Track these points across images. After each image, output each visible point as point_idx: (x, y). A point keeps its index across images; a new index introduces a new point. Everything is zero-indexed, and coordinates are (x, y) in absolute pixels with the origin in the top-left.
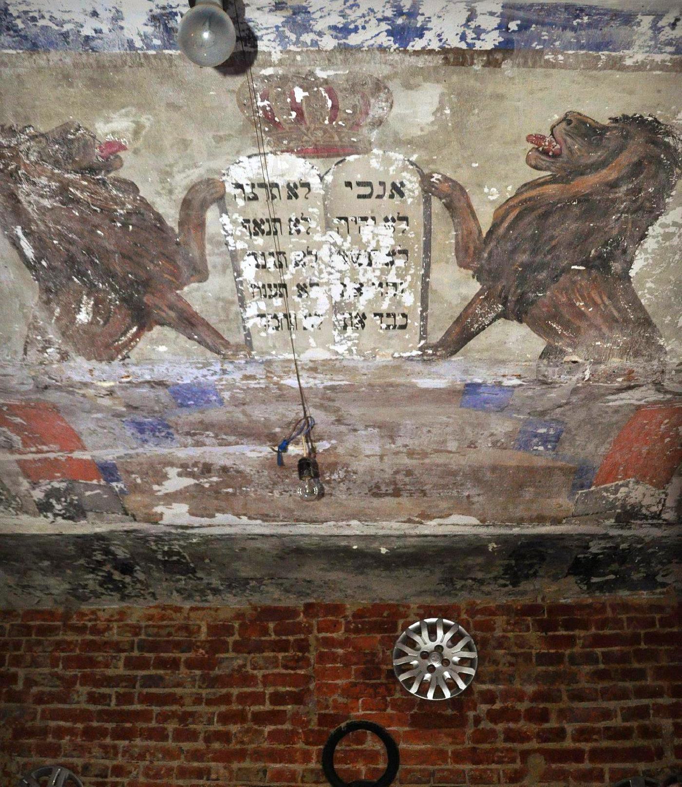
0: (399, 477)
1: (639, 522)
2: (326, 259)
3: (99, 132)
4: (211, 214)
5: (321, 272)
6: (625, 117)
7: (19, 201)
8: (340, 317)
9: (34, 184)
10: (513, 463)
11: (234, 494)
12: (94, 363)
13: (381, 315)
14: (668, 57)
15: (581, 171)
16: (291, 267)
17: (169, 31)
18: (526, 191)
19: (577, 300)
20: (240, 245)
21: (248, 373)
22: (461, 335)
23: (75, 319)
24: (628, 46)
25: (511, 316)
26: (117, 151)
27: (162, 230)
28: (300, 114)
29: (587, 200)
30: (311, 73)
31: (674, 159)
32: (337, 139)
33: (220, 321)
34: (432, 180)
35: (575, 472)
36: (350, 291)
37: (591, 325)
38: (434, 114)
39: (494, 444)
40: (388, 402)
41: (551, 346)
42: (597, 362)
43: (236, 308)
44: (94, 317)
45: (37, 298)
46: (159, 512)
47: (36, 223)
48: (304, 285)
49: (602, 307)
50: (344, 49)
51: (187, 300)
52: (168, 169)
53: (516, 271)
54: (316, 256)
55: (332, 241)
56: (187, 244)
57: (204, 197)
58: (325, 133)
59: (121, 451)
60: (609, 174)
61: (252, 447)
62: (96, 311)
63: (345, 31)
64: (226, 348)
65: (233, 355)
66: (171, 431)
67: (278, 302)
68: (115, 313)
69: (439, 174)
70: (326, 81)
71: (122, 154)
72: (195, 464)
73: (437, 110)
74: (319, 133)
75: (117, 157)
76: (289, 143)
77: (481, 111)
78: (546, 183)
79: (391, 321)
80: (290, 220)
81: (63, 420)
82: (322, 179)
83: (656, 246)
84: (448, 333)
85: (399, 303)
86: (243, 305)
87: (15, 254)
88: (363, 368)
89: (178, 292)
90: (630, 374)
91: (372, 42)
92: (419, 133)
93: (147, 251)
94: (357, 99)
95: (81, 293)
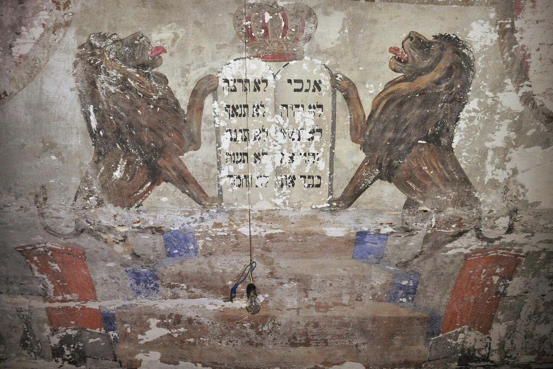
0: (310, 328)
1: (474, 364)
2: (273, 135)
3: (153, 39)
4: (208, 100)
6: (441, 35)
7: (96, 87)
8: (279, 178)
9: (108, 75)
10: (386, 314)
11: (194, 344)
12: (119, 208)
13: (305, 177)
15: (419, 73)
16: (252, 140)
18: (389, 87)
19: (424, 166)
20: (223, 124)
21: (217, 221)
22: (354, 192)
23: (112, 175)
26: (161, 53)
27: (177, 111)
28: (267, 31)
29: (424, 94)
31: (469, 64)
32: (285, 49)
34: (337, 79)
35: (428, 322)
36: (287, 159)
37: (434, 184)
39: (374, 296)
40: (306, 254)
41: (410, 199)
42: (439, 211)
43: (215, 170)
44: (125, 174)
45: (91, 159)
46: (139, 359)
47: (103, 104)
48: (259, 154)
49: (438, 170)
51: (185, 163)
53: (386, 145)
54: (267, 132)
55: (277, 122)
57: (206, 88)
59: (120, 302)
60: (435, 75)
61: (211, 300)
62: (126, 171)
64: (206, 200)
65: (210, 205)
66: (158, 282)
67: (241, 166)
69: (341, 74)
71: (163, 56)
72: (170, 317)
73: (341, 30)
74: (276, 45)
76: (258, 51)
77: (365, 30)
78: (400, 81)
79: (310, 181)
80: (254, 106)
81: (86, 268)
82: (274, 77)
83: (465, 126)
84: (346, 190)
85: (316, 168)
86: (219, 169)
87: (85, 125)
88: (292, 217)
89: (180, 157)
90: (459, 222)
92: (331, 46)
93: (166, 125)
94: (298, 22)
95: (120, 156)
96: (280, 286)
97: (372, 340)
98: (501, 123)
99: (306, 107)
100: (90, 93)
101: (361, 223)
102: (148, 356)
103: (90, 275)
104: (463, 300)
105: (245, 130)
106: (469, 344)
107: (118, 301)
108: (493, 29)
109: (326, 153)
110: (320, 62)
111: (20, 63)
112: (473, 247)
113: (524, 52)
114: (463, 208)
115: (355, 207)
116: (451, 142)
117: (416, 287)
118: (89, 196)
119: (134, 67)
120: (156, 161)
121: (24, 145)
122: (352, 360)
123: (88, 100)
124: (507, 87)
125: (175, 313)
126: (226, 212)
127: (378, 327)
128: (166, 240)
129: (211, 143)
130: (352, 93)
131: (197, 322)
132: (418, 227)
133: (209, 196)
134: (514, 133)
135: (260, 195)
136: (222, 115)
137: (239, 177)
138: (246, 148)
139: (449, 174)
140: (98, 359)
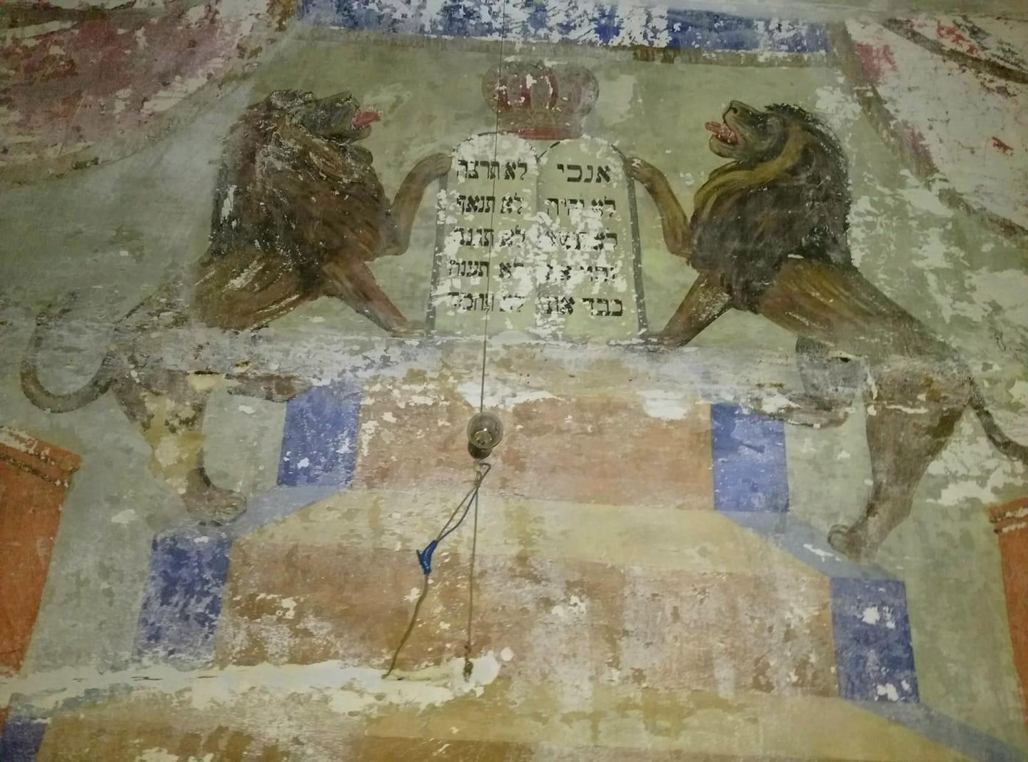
2: (534, 239)
3: (365, 103)
4: (431, 189)
6: (777, 106)
7: (254, 161)
8: (544, 300)
13: (591, 301)
17: (452, 20)
20: (450, 220)
21: (416, 366)
24: (756, 45)
25: (742, 306)
27: (377, 200)
28: (528, 99)
30: (541, 62)
32: (554, 123)
33: (402, 298)
36: (557, 274)
37: (842, 318)
38: (630, 102)
43: (426, 285)
44: (252, 283)
50: (565, 42)
52: (407, 142)
54: (524, 235)
55: (541, 222)
56: (397, 215)
62: (257, 278)
63: (567, 28)
64: (400, 324)
67: (475, 281)
70: (551, 70)
71: (373, 124)
74: (541, 117)
79: (603, 307)
80: (504, 199)
82: (538, 160)
85: (611, 289)
86: (435, 280)
88: (570, 362)
89: (367, 263)
91: (585, 37)
101: (715, 383)
103: (48, 559)
105: (487, 231)
108: (849, 98)
112: (997, 479)
115: (696, 346)
117: (907, 634)
119: (325, 138)
120: (319, 267)
123: (232, 177)
125: (233, 727)
126: (439, 347)
129: (426, 245)
132: (843, 397)
137: (470, 296)
138: (487, 255)
139: (866, 304)
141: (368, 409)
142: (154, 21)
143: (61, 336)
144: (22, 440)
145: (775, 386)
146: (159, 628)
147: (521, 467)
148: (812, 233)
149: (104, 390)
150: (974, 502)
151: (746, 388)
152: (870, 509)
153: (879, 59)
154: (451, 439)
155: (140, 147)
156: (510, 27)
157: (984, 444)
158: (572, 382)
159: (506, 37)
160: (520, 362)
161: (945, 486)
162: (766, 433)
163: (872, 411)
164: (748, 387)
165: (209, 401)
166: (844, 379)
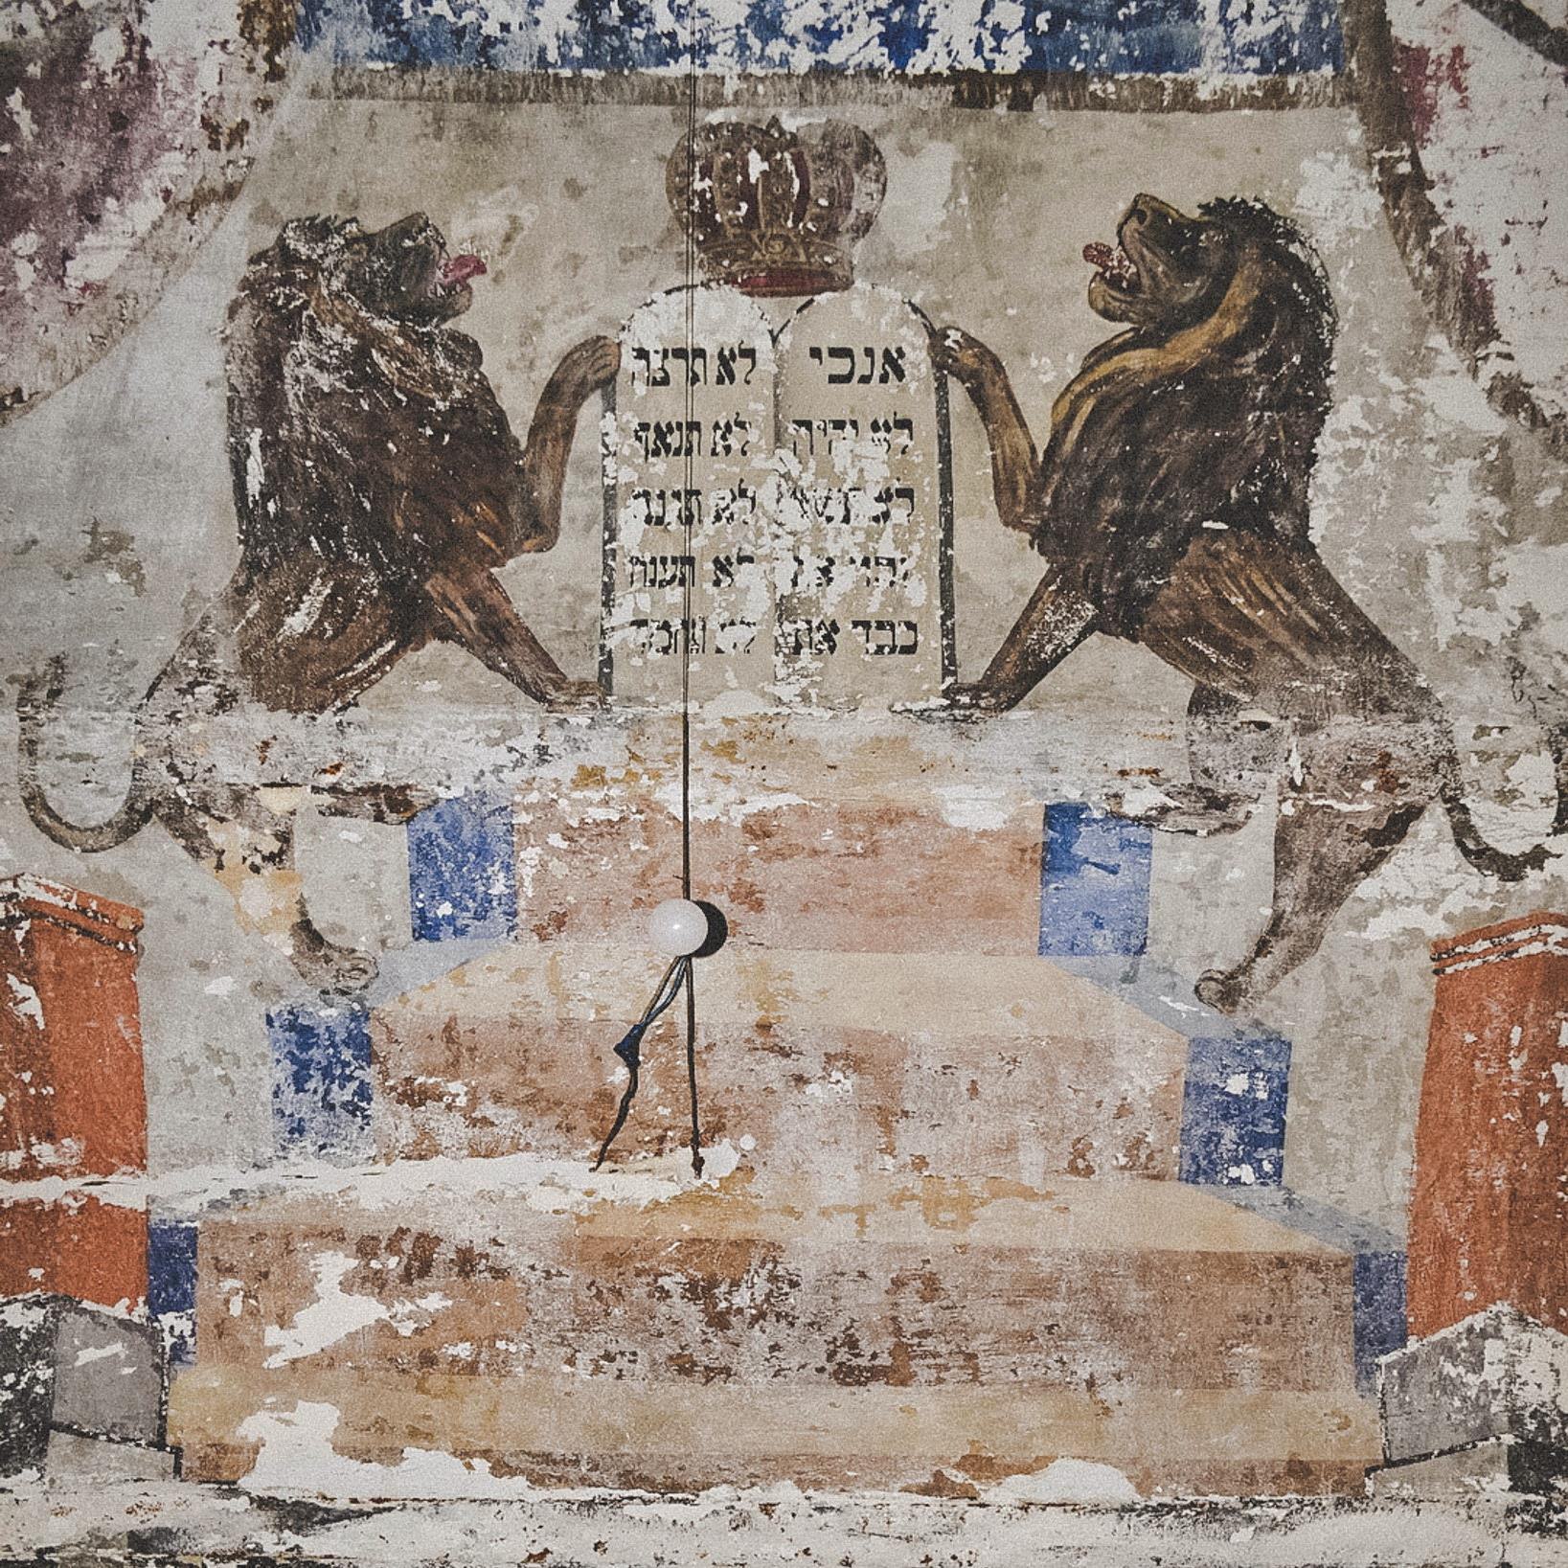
2: (771, 507)
5: (759, 533)
7: (281, 377)
8: (788, 627)
9: (318, 339)
11: (472, 1368)
13: (866, 625)
14: (1253, 79)
16: (708, 520)
18: (1098, 363)
20: (626, 475)
21: (590, 761)
23: (281, 624)
24: (1195, 59)
26: (469, 275)
28: (753, 211)
30: (775, 122)
32: (803, 258)
34: (948, 343)
36: (810, 575)
37: (1273, 646)
43: (595, 608)
44: (319, 622)
47: (291, 424)
48: (727, 559)
50: (823, 72)
54: (753, 499)
57: (584, 376)
58: (786, 244)
59: (221, 1178)
62: (327, 610)
66: (370, 1074)
67: (674, 594)
68: (363, 613)
71: (474, 282)
73: (950, 199)
75: (467, 288)
77: (1012, 197)
78: (1122, 348)
79: (885, 638)
80: (717, 426)
82: (775, 340)
84: (997, 663)
85: (900, 603)
88: (829, 744)
96: (794, 1096)
97: (1145, 1358)
98: (1448, 467)
99: (864, 425)
100: (260, 399)
101: (1055, 770)
102: (288, 1423)
103: (139, 1042)
104: (1467, 1185)
106: (1532, 1388)
107: (218, 1170)
108: (1363, 178)
109: (929, 560)
110: (899, 296)
111: (80, 306)
112: (1455, 903)
113: (1467, 249)
114: (1385, 717)
116: (1303, 527)
117: (1282, 1106)
118: (193, 685)
121: (35, 542)
122: (1077, 1450)
123: (250, 414)
124: (1440, 360)
125: (415, 1229)
127: (1163, 1301)
128: (422, 850)
129: (588, 529)
130: (994, 384)
131: (491, 1269)
132: (1248, 789)
133: (571, 678)
134: (1495, 500)
135: (730, 675)
136: (626, 451)
137: (666, 626)
139: (1317, 618)
140: (95, 1436)
141: (526, 831)
142: (34, 70)
143: (61, 737)
144: (56, 892)
145: (1148, 772)
146: (301, 1120)
147: (758, 906)
148: (1250, 478)
149: (146, 817)
150: (1414, 934)
151: (1101, 778)
152: (1262, 948)
153: (1440, 81)
154: (653, 868)
155: (85, 358)
156: (712, 41)
157: (1450, 853)
158: (833, 776)
159: (704, 65)
160: (754, 743)
161: (1376, 914)
162: (1125, 845)
163: (1288, 809)
164: (1106, 776)
165: (295, 827)
166: (1255, 759)
